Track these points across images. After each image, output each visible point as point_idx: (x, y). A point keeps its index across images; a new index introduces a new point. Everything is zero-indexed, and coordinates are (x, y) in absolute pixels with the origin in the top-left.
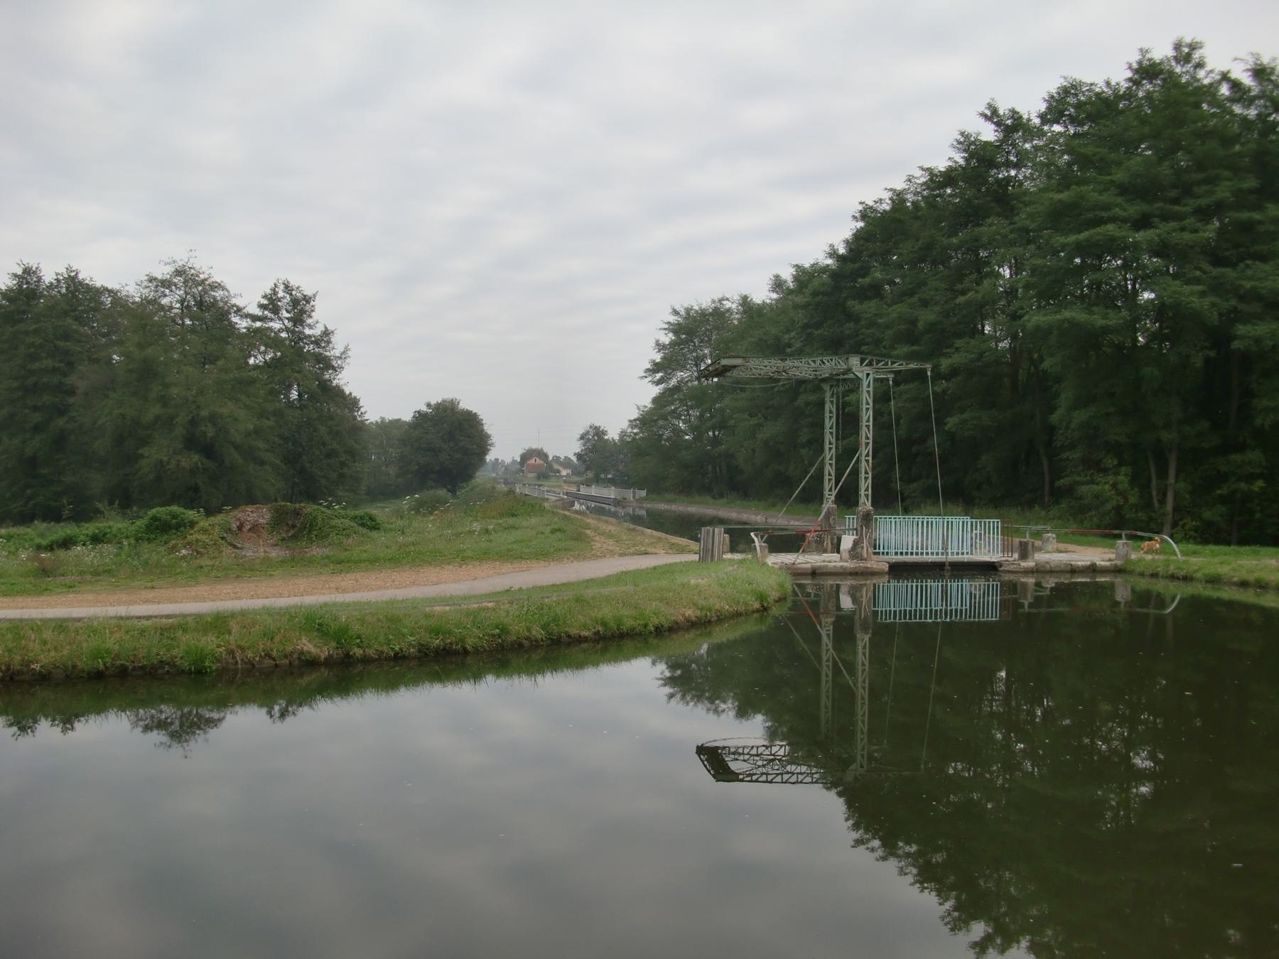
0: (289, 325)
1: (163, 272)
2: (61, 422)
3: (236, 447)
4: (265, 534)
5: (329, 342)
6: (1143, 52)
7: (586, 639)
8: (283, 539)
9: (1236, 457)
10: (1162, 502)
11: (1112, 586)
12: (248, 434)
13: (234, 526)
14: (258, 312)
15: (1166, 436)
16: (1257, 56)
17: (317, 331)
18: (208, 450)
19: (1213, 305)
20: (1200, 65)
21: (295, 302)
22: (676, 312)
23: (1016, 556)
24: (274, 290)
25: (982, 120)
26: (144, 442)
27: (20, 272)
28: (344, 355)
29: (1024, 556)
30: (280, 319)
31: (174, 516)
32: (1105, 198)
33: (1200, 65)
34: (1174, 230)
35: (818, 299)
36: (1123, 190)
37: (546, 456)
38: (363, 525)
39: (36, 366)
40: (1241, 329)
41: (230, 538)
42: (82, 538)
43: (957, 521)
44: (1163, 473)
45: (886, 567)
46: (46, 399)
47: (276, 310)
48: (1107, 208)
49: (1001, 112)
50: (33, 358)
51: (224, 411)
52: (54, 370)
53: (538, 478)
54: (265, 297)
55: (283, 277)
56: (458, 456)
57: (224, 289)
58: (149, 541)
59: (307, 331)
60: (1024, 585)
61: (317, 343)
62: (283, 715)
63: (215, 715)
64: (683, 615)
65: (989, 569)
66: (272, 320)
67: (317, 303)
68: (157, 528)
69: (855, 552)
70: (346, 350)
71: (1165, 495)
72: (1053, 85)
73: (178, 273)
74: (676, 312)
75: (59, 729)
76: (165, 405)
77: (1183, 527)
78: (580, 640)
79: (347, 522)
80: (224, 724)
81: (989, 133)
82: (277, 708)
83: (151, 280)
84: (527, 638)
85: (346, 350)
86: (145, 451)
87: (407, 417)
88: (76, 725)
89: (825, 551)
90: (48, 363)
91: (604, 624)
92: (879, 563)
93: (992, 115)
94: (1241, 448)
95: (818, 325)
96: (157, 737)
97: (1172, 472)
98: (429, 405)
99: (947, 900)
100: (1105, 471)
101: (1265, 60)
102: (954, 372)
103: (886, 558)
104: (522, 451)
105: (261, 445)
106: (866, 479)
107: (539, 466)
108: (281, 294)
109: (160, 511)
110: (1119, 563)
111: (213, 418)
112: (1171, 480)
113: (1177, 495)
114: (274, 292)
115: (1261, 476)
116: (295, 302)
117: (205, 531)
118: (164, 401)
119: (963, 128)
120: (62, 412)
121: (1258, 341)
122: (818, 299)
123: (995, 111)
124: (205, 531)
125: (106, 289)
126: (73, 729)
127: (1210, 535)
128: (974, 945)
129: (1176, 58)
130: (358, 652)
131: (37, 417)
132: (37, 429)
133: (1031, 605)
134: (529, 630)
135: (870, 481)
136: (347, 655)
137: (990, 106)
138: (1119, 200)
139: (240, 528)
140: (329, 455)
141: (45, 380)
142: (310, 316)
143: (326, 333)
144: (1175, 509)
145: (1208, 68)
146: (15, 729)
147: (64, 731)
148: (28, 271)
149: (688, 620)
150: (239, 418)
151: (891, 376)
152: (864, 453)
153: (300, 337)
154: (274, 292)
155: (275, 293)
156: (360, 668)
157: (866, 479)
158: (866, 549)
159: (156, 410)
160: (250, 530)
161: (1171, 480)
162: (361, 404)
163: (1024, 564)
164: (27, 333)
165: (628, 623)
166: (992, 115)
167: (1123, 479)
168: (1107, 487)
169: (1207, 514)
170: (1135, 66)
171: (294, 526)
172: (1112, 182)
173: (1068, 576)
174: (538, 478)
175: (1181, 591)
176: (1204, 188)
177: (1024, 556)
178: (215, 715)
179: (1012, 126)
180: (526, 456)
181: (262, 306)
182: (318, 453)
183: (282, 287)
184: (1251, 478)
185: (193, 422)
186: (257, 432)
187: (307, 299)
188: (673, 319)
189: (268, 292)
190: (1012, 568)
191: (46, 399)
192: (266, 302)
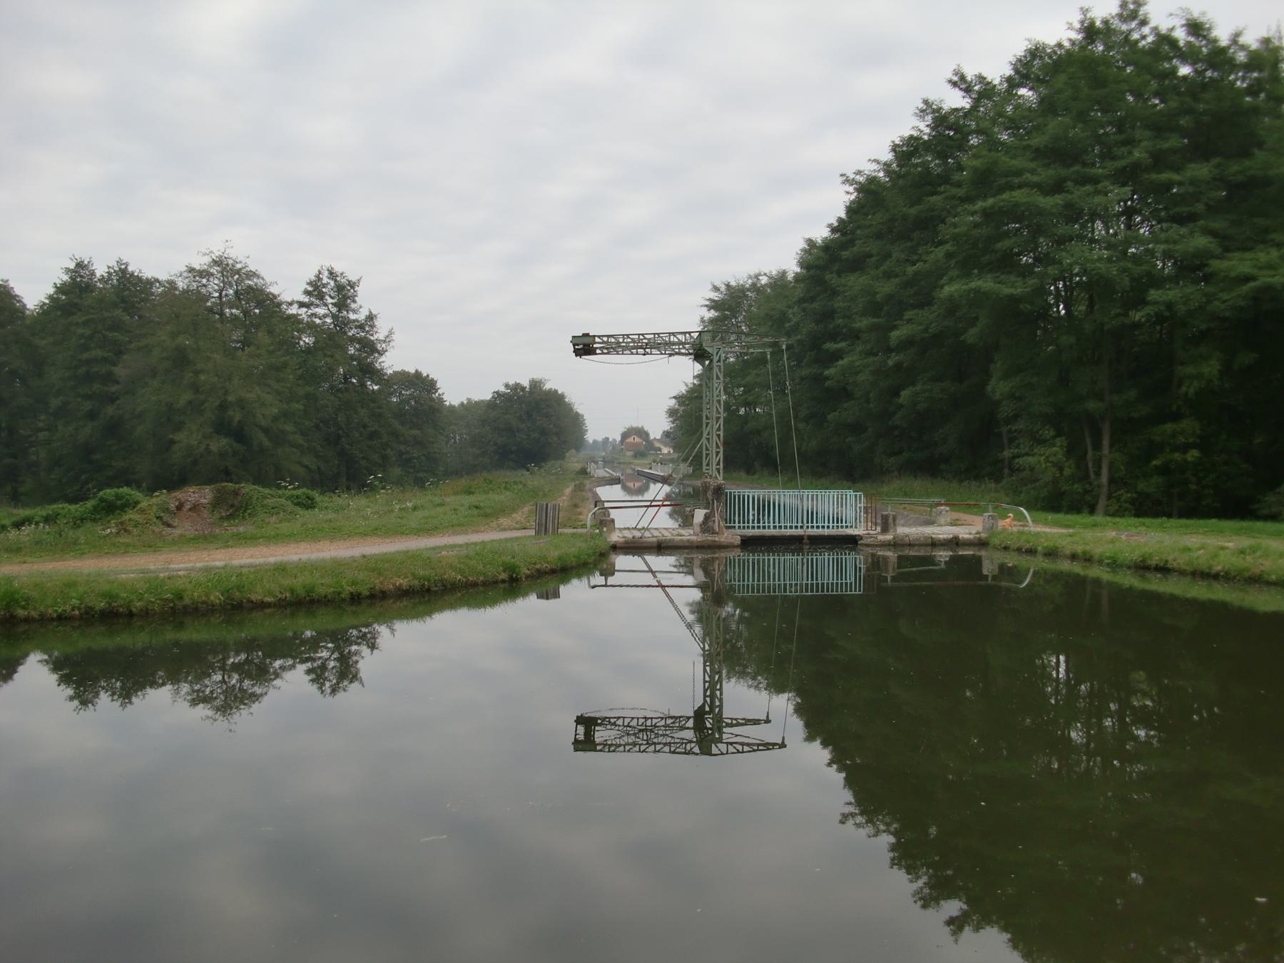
0: (334, 310)
1: (200, 262)
2: (110, 410)
3: (266, 431)
4: (206, 513)
5: (372, 326)
6: (1084, 11)
7: (269, 605)
8: (222, 518)
9: (1169, 427)
10: (1098, 474)
11: (977, 561)
12: (275, 419)
13: (172, 506)
14: (306, 299)
15: (1092, 405)
16: (1187, 10)
17: (361, 316)
18: (239, 435)
19: (1125, 270)
20: (1144, 23)
21: (340, 288)
22: (716, 289)
23: (879, 529)
24: (318, 276)
25: (949, 86)
26: (179, 427)
27: (72, 266)
28: (388, 340)
29: (885, 530)
30: (326, 305)
31: (118, 497)
32: (1017, 163)
33: (1144, 23)
34: (1088, 195)
35: (812, 272)
36: (1038, 153)
37: (647, 434)
38: (298, 504)
39: (85, 356)
40: (1154, 294)
41: (166, 517)
42: (37, 519)
43: (850, 493)
44: (1097, 446)
45: (738, 541)
46: (96, 387)
47: (321, 296)
48: (1019, 173)
49: (969, 79)
50: (86, 348)
51: (251, 396)
52: (105, 360)
53: (635, 456)
54: (310, 283)
55: (327, 264)
56: (535, 435)
58: (94, 520)
59: (352, 316)
60: (885, 558)
61: (361, 327)
62: (334, 690)
63: (257, 690)
64: (394, 585)
65: (851, 542)
66: (318, 306)
67: (360, 290)
68: (103, 509)
69: (706, 526)
70: (391, 332)
71: (1100, 468)
72: (1019, 49)
73: (216, 263)
74: (716, 289)
75: (119, 703)
76: (197, 391)
77: (1118, 500)
78: (262, 605)
81: (956, 100)
82: (328, 684)
83: (191, 270)
84: (203, 603)
85: (391, 332)
86: (179, 436)
87: (488, 396)
88: (134, 699)
90: (99, 353)
91: (292, 591)
92: (731, 536)
93: (959, 81)
94: (1176, 417)
95: (813, 299)
96: (203, 711)
97: (1106, 442)
98: (507, 386)
99: (918, 878)
100: (1041, 442)
101: (1196, 15)
102: (907, 343)
103: (738, 531)
104: (623, 430)
105: (289, 428)
106: (717, 453)
107: (637, 444)
108: (325, 280)
109: (108, 493)
110: (983, 535)
111: (241, 403)
112: (1106, 450)
113: (1111, 465)
114: (319, 278)
115: (1194, 446)
116: (340, 288)
117: (142, 511)
118: (195, 387)
119: (925, 97)
120: (112, 399)
121: (1169, 306)
122: (812, 272)
123: (963, 78)
124: (142, 511)
125: (157, 280)
126: (131, 703)
127: (1146, 508)
128: (950, 922)
129: (1120, 16)
130: (21, 613)
131: (87, 406)
132: (92, 415)
133: (894, 579)
134: (207, 595)
135: (721, 455)
136: (13, 616)
137: (956, 73)
138: (1032, 165)
139: (179, 508)
140: (374, 435)
141: (95, 369)
142: (354, 301)
143: (371, 317)
144: (1111, 481)
145: (1152, 24)
146: (76, 703)
147: (123, 705)
149: (399, 589)
150: (266, 404)
151: (768, 351)
153: (347, 323)
154: (319, 278)
155: (320, 279)
156: (21, 628)
157: (717, 453)
158: (717, 522)
159: (187, 396)
160: (190, 510)
161: (1106, 450)
162: (438, 385)
163: (881, 537)
164: (77, 324)
165: (322, 591)
166: (959, 81)
167: (1057, 450)
168: (1042, 458)
169: (1142, 486)
170: (1078, 26)
171: (232, 506)
172: (1029, 146)
173: (929, 549)
174: (635, 456)
175: (1035, 564)
176: (1124, 150)
177: (885, 530)
178: (257, 690)
179: (982, 92)
180: (625, 436)
181: (307, 293)
182: (357, 435)
183: (326, 273)
184: (1185, 448)
185: (223, 407)
186: (285, 415)
187: (352, 285)
188: (715, 296)
189: (313, 278)
190: (869, 541)
191: (96, 387)
192: (310, 289)
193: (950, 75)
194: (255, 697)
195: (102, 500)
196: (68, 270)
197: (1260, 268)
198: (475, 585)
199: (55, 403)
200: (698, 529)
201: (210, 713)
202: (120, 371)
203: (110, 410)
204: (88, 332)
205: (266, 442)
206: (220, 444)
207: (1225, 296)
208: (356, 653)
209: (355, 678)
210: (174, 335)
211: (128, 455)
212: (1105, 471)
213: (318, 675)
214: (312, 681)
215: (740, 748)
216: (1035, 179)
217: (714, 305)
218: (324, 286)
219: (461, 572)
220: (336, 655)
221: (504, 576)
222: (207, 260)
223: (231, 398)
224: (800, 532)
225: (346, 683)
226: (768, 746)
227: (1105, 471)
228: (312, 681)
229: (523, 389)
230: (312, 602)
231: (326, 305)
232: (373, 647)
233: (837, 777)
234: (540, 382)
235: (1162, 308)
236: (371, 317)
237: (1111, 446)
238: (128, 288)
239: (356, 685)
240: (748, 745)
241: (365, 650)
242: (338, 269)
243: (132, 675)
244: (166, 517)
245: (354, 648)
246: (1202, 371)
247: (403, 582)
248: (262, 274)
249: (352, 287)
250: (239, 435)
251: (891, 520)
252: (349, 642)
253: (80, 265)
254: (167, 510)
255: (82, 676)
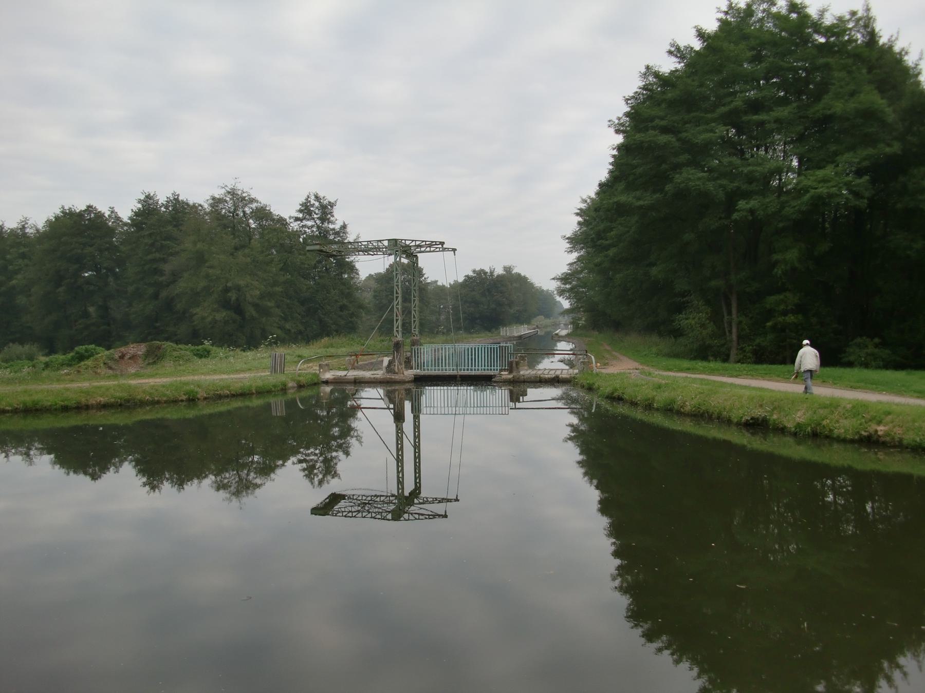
0: (318, 222)
1: (219, 193)
3: (256, 306)
4: (140, 361)
7: (8, 411)
10: (730, 332)
13: (117, 356)
14: (301, 215)
17: (337, 227)
19: (721, 186)
24: (307, 199)
27: (142, 197)
30: (313, 219)
31: (86, 351)
39: (150, 257)
40: (742, 204)
41: (111, 363)
47: (310, 213)
54: (302, 205)
55: (313, 190)
56: (493, 306)
57: (257, 201)
59: (331, 226)
61: (337, 233)
63: (258, 481)
79: (188, 353)
80: (263, 488)
82: (316, 479)
89: (412, 368)
96: (222, 494)
97: (734, 311)
98: (474, 271)
111: (238, 288)
112: (734, 316)
121: (752, 211)
131: (151, 291)
137: (672, 45)
139: (122, 357)
140: (342, 308)
142: (333, 216)
143: (344, 227)
144: (739, 337)
148: (148, 197)
152: (395, 303)
153: (327, 231)
159: (203, 284)
160: (130, 358)
162: (424, 272)
176: (729, 99)
181: (300, 211)
183: (313, 197)
185: (227, 290)
187: (332, 205)
188: (583, 206)
193: (668, 48)
194: (257, 486)
195: (77, 353)
196: (140, 201)
197: (820, 182)
198: (158, 402)
199: (131, 289)
200: (384, 370)
201: (228, 495)
202: (167, 268)
203: (164, 294)
204: (150, 242)
205: (254, 313)
206: (221, 315)
207: (794, 203)
208: (335, 458)
209: (335, 475)
210: (195, 243)
211: (177, 324)
212: (734, 330)
213: (309, 472)
214: (306, 475)
215: (417, 516)
216: (663, 123)
217: (581, 213)
218: (313, 205)
219: (150, 394)
220: (321, 459)
221: (184, 398)
222: (223, 191)
223: (229, 284)
224: (455, 373)
225: (329, 477)
226: (435, 516)
227: (734, 330)
228: (306, 475)
229: (485, 273)
230: (37, 410)
231: (313, 219)
232: (347, 454)
233: (607, 545)
234: (510, 268)
235: (745, 214)
236: (344, 227)
237: (738, 311)
238: (180, 211)
239: (336, 479)
240: (422, 515)
241: (340, 454)
242: (321, 195)
243: (184, 473)
244: (111, 363)
245: (334, 454)
246: (790, 255)
247: (102, 400)
248: (259, 199)
249: (332, 207)
250: (238, 309)
251: (514, 365)
252: (330, 449)
253: (148, 197)
254: (112, 359)
255: (152, 473)
